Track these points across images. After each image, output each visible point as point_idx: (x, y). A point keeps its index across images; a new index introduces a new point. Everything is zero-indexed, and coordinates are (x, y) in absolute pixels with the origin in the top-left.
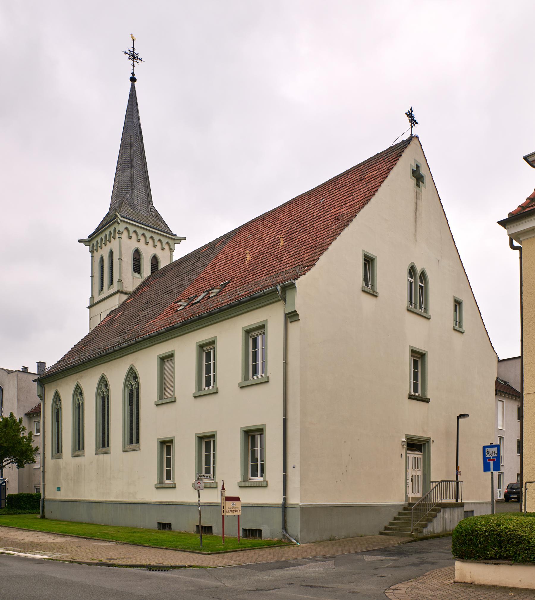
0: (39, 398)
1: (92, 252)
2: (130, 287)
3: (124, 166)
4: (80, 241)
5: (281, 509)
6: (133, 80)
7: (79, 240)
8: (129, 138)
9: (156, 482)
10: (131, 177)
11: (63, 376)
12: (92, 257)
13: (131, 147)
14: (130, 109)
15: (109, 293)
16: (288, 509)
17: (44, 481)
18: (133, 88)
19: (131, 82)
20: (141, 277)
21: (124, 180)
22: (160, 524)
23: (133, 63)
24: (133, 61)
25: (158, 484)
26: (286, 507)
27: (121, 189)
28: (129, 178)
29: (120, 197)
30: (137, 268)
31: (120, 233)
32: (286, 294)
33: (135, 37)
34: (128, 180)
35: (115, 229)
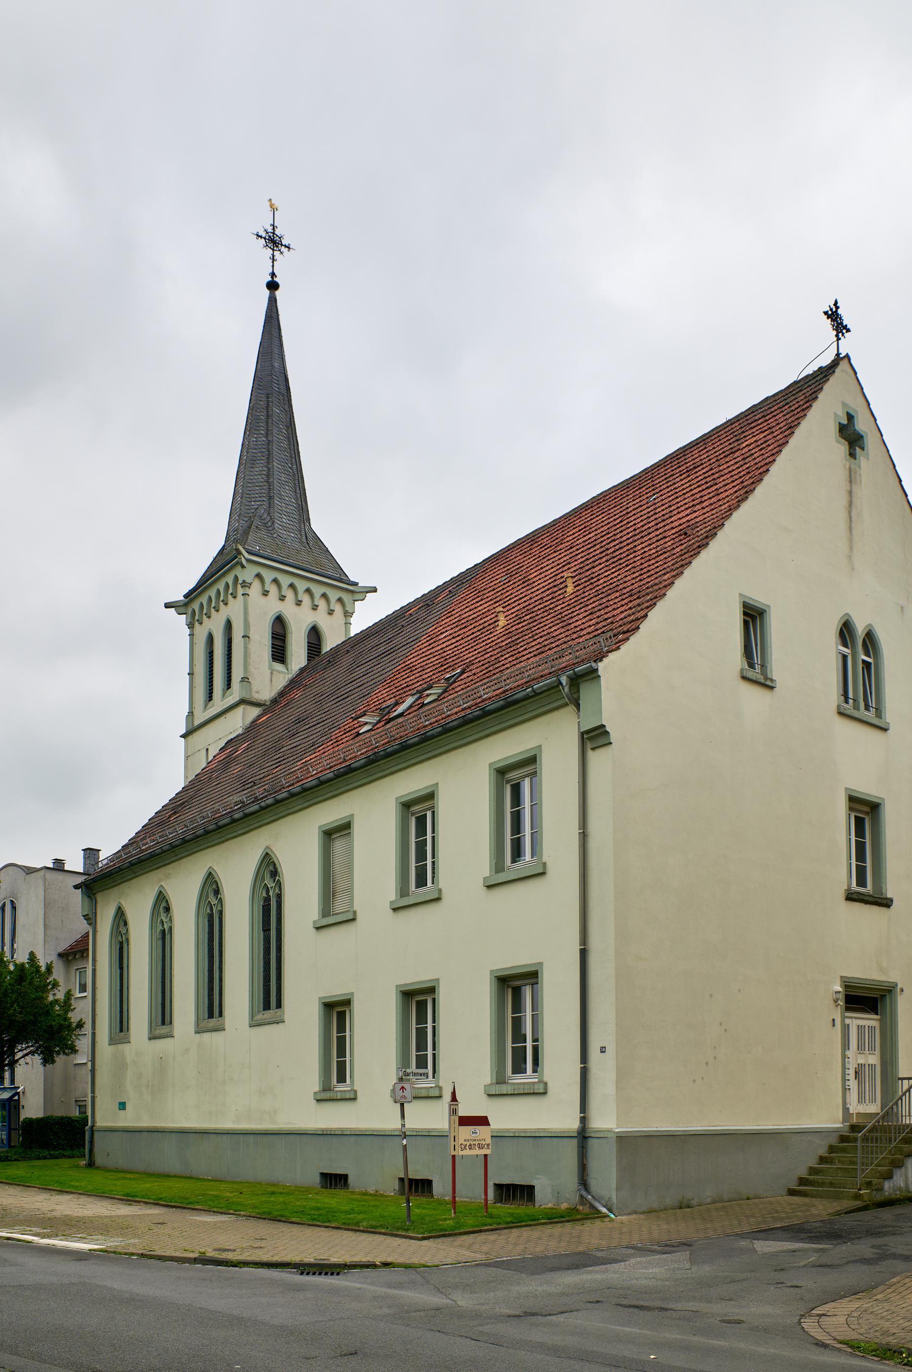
1: (191, 625)
3: (253, 455)
4: (168, 606)
6: (273, 286)
11: (133, 875)
12: (191, 635)
13: (268, 416)
17: (93, 1091)
19: (268, 292)
20: (287, 669)
28: (263, 476)
34: (262, 480)
35: (236, 578)
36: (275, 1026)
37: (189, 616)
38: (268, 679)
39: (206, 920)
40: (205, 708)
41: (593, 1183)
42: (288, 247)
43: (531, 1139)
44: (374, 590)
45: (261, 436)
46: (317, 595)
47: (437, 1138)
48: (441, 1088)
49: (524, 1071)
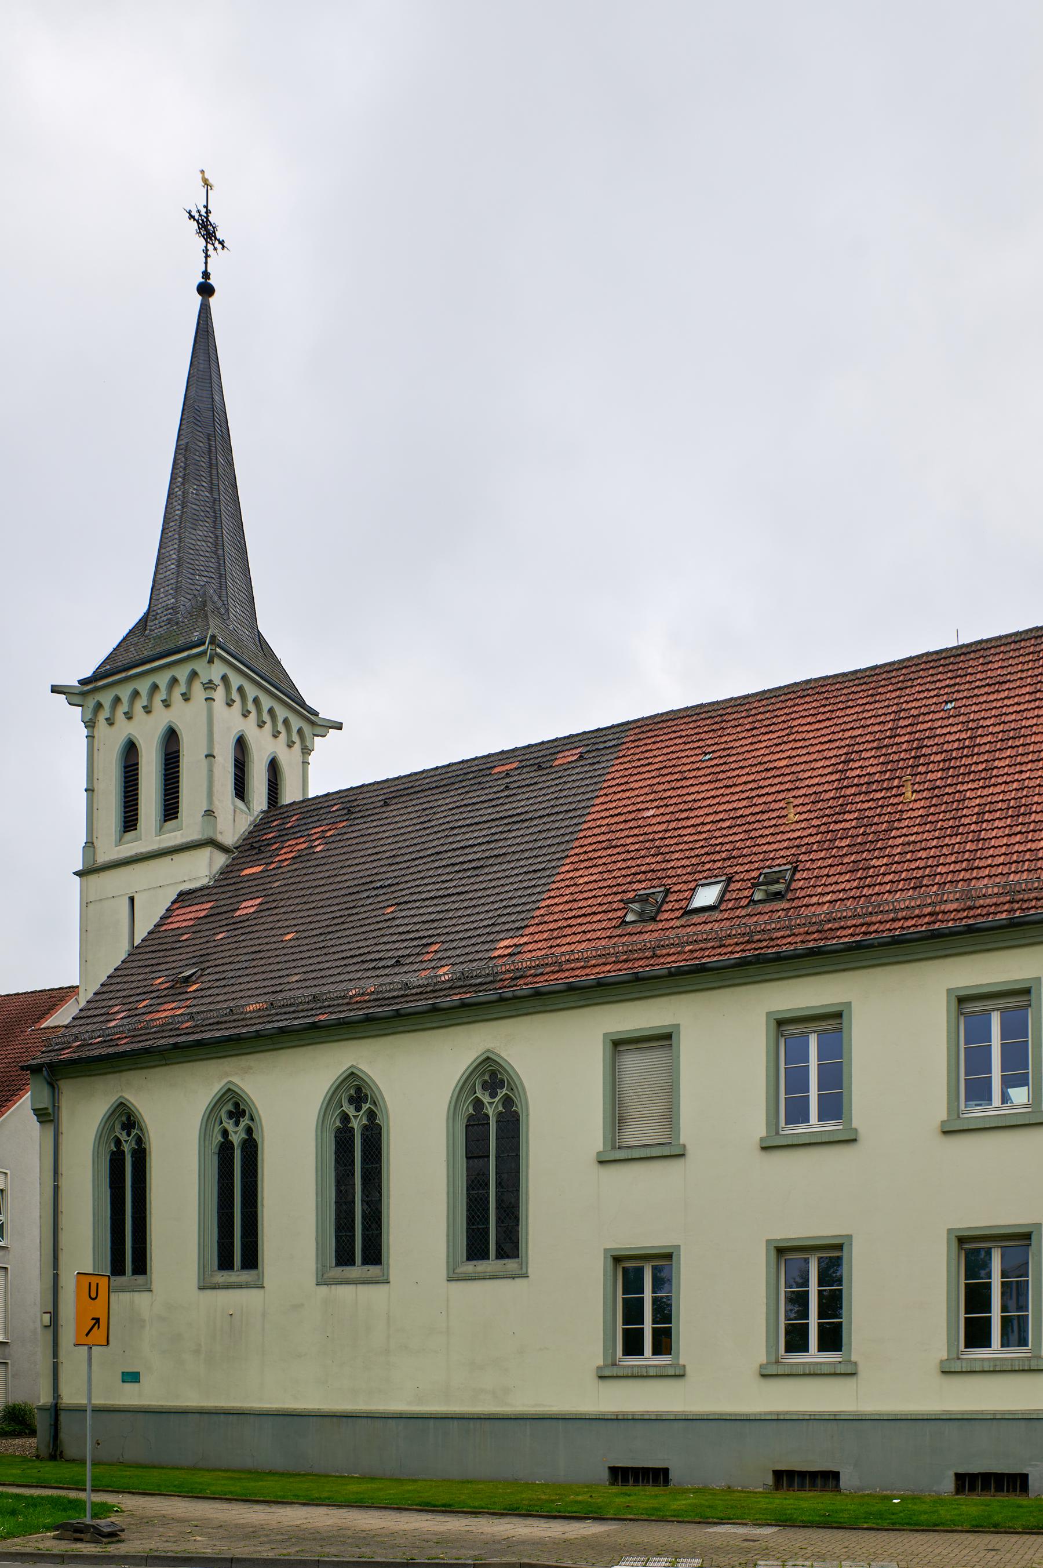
0: (35, 1117)
1: (90, 724)
2: (230, 836)
3: (194, 512)
4: (55, 689)
6: (206, 290)
7: (52, 686)
8: (205, 440)
9: (763, 1359)
11: (164, 1062)
12: (90, 737)
13: (211, 466)
14: (202, 366)
15: (160, 841)
18: (205, 314)
19: (200, 298)
20: (249, 809)
21: (197, 547)
23: (206, 247)
24: (207, 242)
25: (605, 1366)
27: (191, 571)
28: (209, 544)
29: (189, 591)
30: (241, 790)
31: (209, 686)
33: (211, 181)
34: (209, 550)
35: (194, 674)
36: (510, 1280)
37: (90, 710)
38: (231, 817)
39: (333, 1135)
40: (120, 840)
42: (221, 243)
43: (1023, 1423)
44: (339, 726)
45: (203, 489)
47: (850, 1422)
48: (856, 1363)
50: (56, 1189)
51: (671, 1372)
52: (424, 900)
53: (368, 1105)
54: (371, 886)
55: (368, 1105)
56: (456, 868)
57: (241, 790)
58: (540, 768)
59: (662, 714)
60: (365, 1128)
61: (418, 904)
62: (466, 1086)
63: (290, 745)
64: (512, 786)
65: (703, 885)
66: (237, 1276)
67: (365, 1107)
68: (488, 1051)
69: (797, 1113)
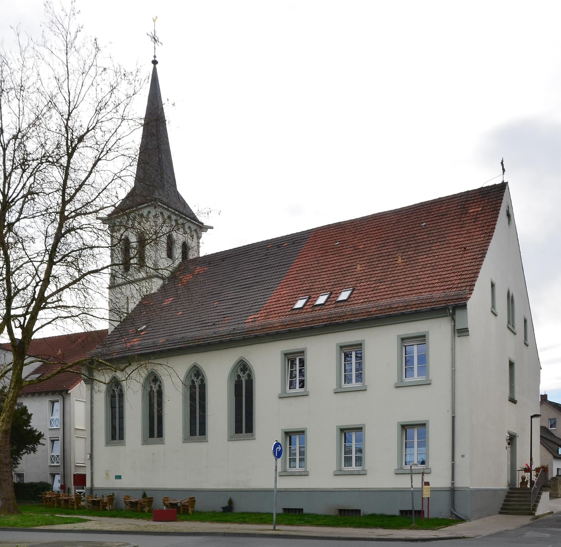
5: (448, 493)
6: (155, 62)
9: (335, 469)
10: (159, 161)
16: (456, 492)
17: (92, 469)
22: (285, 510)
26: (454, 491)
32: (455, 312)
41: (457, 508)
44: (212, 228)
46: (186, 227)
49: (351, 465)
50: (92, 408)
51: (304, 474)
52: (228, 299)
53: (201, 377)
54: (213, 293)
55: (201, 377)
56: (242, 287)
57: (170, 255)
58: (279, 247)
59: (315, 229)
60: (246, 381)
61: (226, 301)
62: (234, 370)
63: (192, 236)
64: (267, 254)
65: (300, 299)
66: (155, 439)
67: (200, 378)
68: (242, 357)
69: (348, 380)
